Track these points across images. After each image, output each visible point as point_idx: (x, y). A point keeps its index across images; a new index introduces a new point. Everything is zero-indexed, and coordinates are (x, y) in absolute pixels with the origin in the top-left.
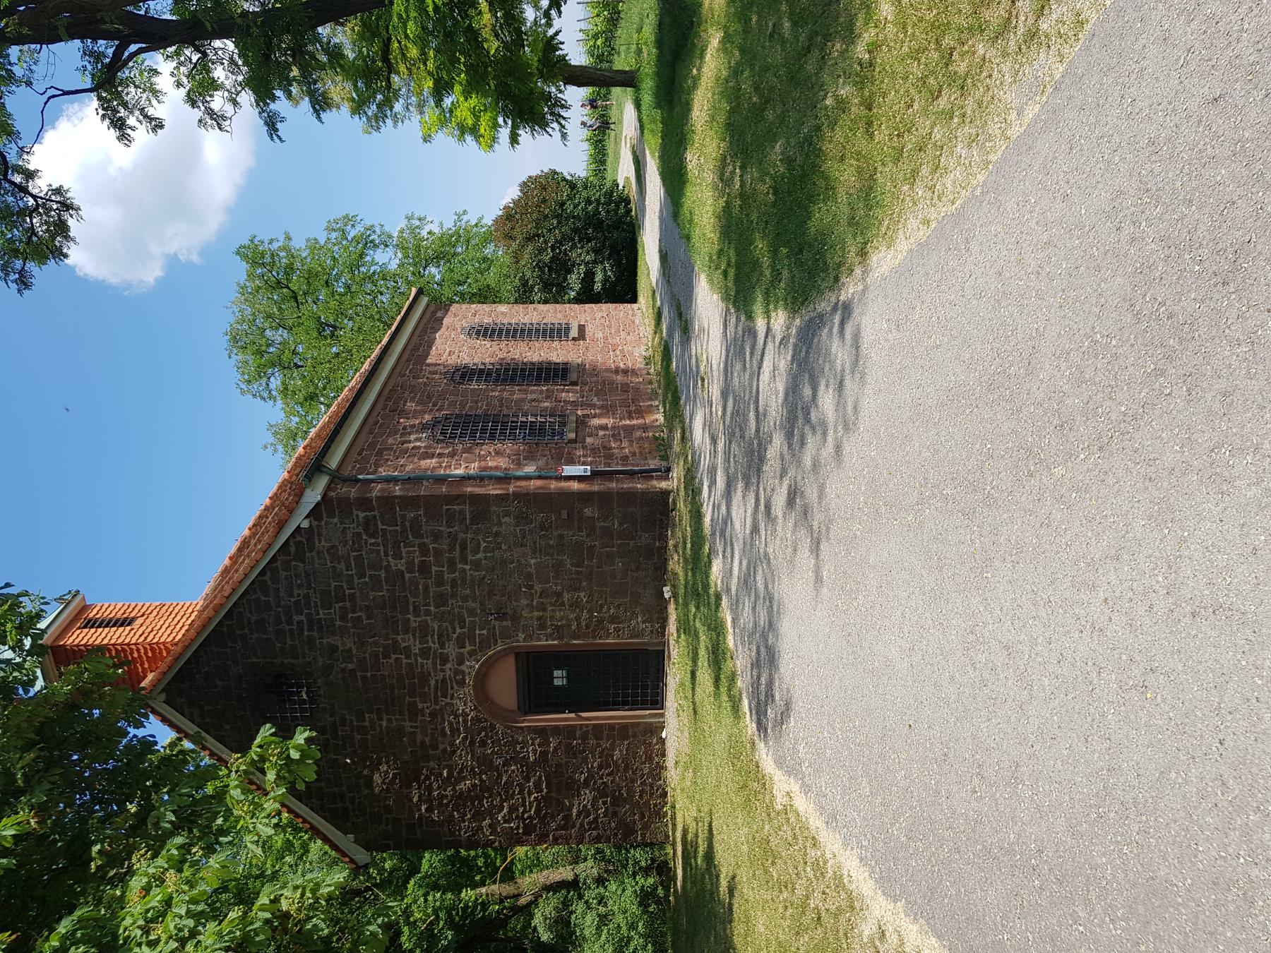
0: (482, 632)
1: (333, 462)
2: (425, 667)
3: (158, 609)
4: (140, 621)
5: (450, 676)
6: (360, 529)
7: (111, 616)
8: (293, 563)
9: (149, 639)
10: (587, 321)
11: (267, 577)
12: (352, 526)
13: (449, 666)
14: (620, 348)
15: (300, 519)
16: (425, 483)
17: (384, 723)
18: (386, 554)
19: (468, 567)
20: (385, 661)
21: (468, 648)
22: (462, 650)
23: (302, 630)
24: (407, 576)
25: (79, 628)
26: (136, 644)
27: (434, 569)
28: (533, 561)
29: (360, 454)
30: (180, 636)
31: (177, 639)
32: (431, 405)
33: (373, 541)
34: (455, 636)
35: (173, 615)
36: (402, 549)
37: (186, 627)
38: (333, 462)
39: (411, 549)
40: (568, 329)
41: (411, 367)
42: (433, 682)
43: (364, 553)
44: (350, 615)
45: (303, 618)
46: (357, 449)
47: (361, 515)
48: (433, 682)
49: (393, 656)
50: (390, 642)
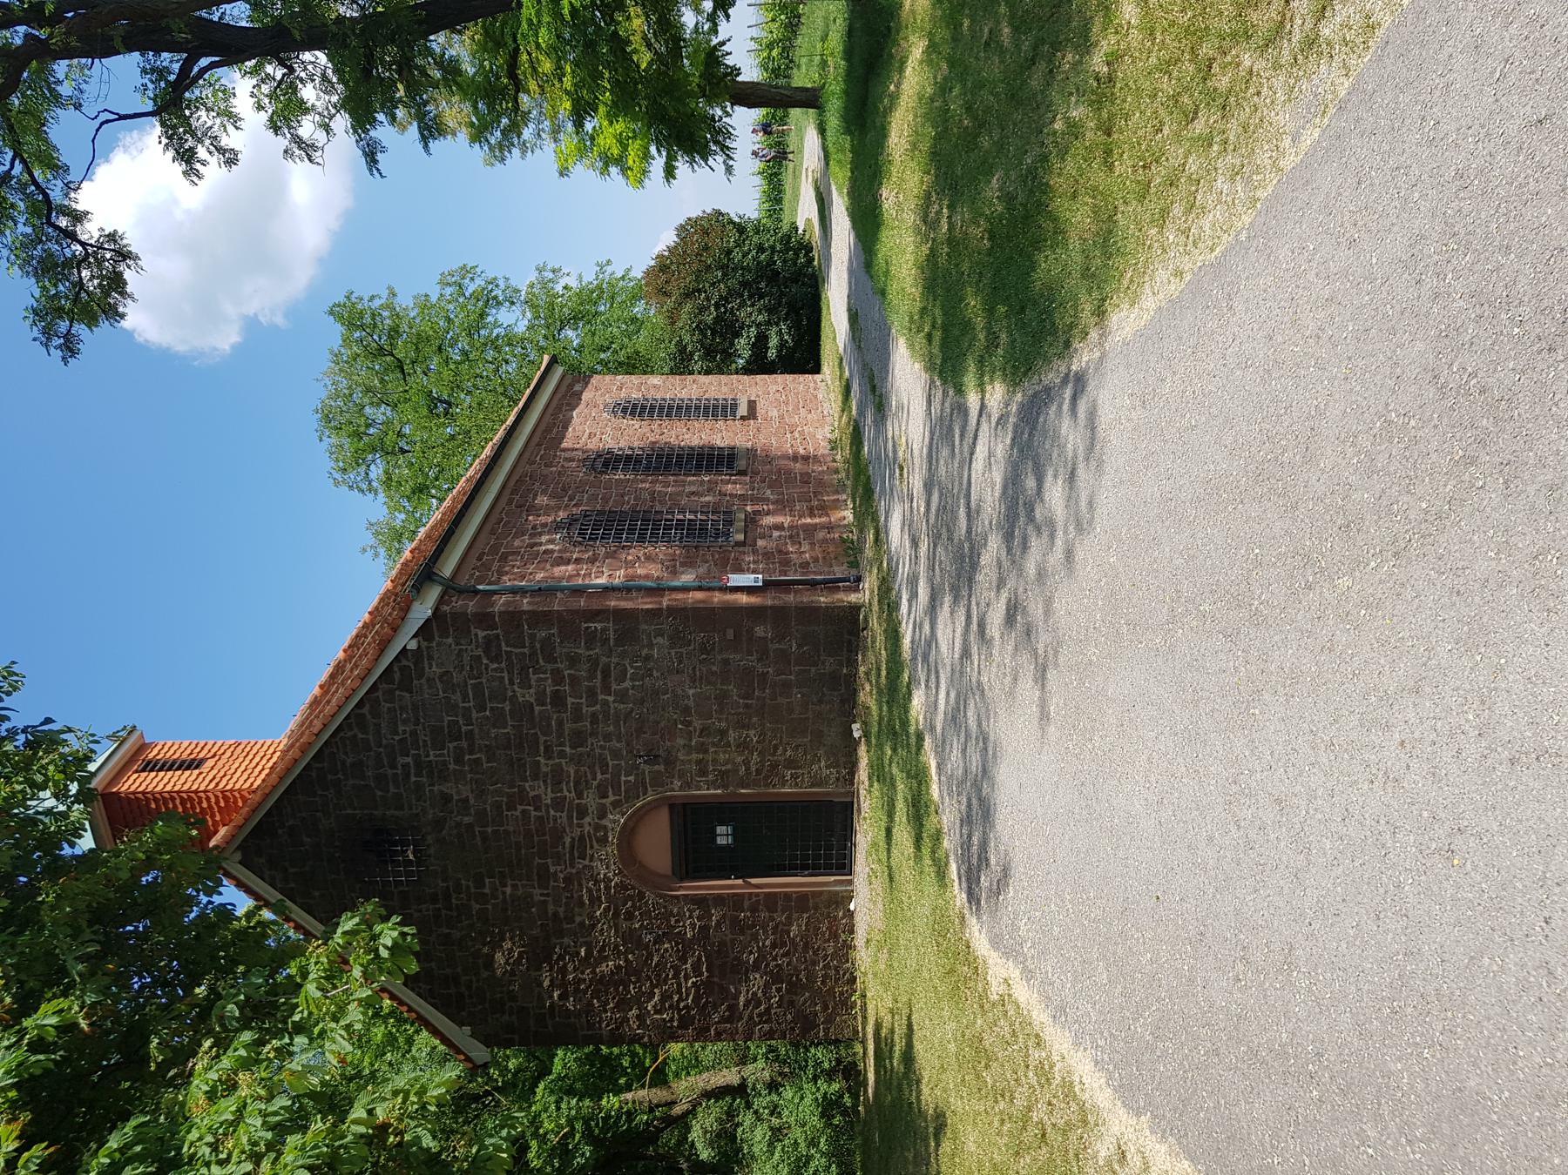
0: (629, 778)
1: (447, 568)
2: (559, 821)
3: (232, 749)
4: (210, 763)
5: (589, 832)
6: (479, 652)
7: (175, 757)
8: (397, 693)
9: (221, 786)
10: (758, 396)
11: (366, 710)
12: (469, 648)
13: (587, 819)
14: (799, 429)
15: (405, 639)
16: (559, 594)
17: (508, 890)
18: (512, 683)
19: (611, 699)
20: (509, 813)
21: (612, 798)
22: (604, 801)
23: (408, 775)
24: (537, 709)
25: (136, 772)
26: (205, 791)
27: (570, 700)
28: (691, 692)
29: (479, 559)
30: (259, 782)
31: (255, 786)
32: (566, 499)
33: (495, 665)
34: (595, 783)
35: (250, 756)
36: (531, 676)
37: (267, 771)
38: (447, 568)
39: (541, 676)
40: (735, 406)
41: (542, 452)
42: (568, 840)
43: (484, 681)
44: (467, 757)
45: (409, 760)
46: (475, 553)
47: (481, 634)
48: (568, 840)
49: (520, 808)
50: (516, 790)
